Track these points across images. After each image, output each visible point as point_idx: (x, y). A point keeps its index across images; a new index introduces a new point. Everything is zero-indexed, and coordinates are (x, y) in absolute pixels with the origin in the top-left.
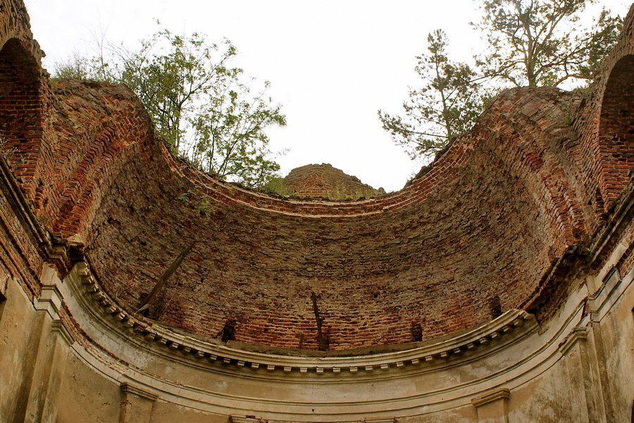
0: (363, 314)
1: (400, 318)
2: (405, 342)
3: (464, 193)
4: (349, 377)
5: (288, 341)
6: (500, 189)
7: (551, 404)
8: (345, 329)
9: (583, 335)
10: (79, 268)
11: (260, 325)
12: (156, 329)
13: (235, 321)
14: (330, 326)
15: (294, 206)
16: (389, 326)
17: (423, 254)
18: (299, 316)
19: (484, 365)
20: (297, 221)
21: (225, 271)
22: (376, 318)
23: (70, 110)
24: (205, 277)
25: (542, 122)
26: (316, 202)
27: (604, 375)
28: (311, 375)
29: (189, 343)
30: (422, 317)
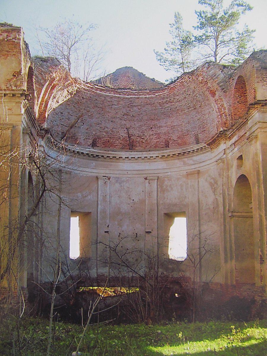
0: (146, 135)
1: (161, 137)
2: (163, 147)
3: (187, 94)
4: (141, 160)
5: (117, 145)
6: (201, 96)
7: (213, 178)
8: (139, 141)
9: (223, 160)
10: (47, 135)
11: (106, 140)
12: (70, 147)
13: (97, 139)
14: (133, 140)
15: (119, 92)
16: (156, 140)
17: (171, 113)
18: (121, 136)
19: (192, 159)
20: (121, 98)
21: (92, 119)
22: (151, 137)
23: (39, 74)
24: (84, 123)
25: (216, 80)
26: (128, 91)
27: (228, 175)
28: (126, 159)
29: (81, 151)
30: (169, 138)
